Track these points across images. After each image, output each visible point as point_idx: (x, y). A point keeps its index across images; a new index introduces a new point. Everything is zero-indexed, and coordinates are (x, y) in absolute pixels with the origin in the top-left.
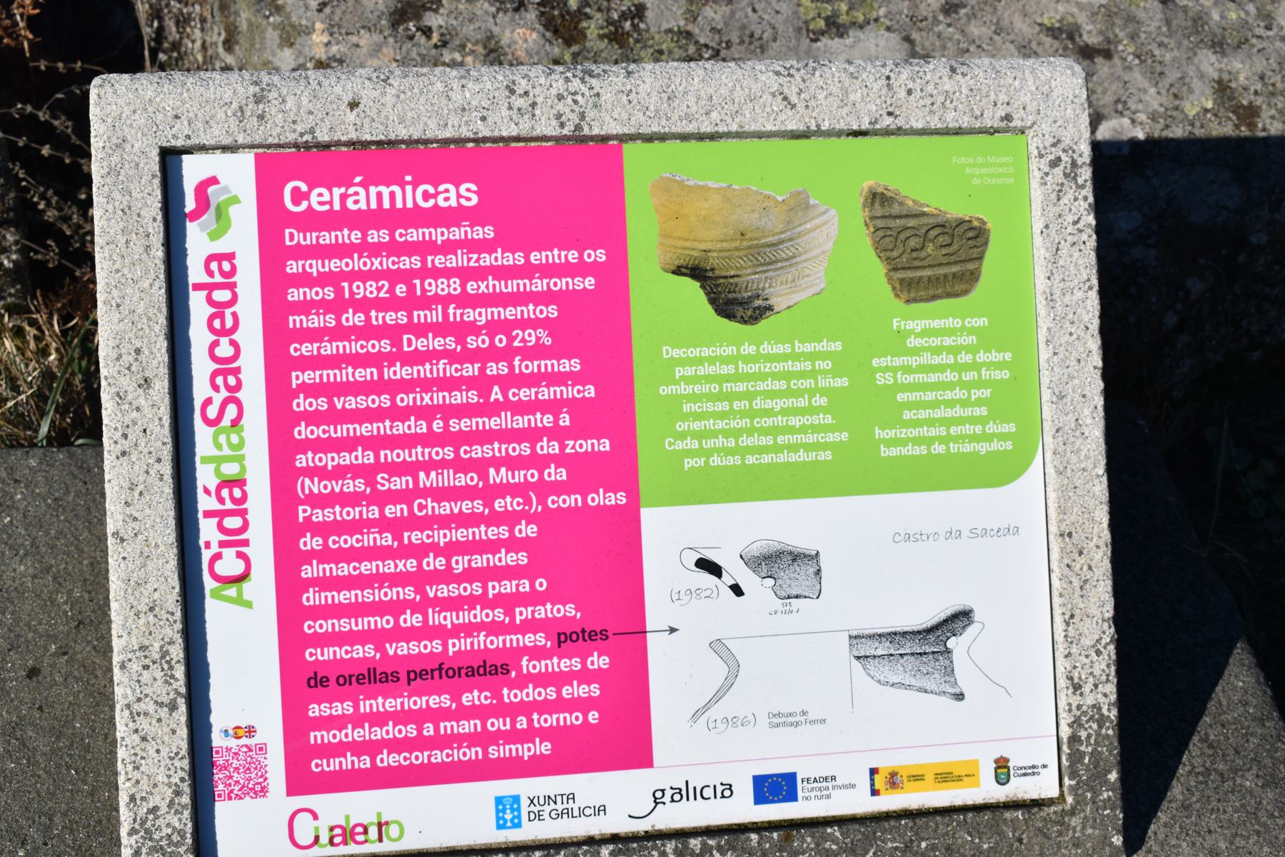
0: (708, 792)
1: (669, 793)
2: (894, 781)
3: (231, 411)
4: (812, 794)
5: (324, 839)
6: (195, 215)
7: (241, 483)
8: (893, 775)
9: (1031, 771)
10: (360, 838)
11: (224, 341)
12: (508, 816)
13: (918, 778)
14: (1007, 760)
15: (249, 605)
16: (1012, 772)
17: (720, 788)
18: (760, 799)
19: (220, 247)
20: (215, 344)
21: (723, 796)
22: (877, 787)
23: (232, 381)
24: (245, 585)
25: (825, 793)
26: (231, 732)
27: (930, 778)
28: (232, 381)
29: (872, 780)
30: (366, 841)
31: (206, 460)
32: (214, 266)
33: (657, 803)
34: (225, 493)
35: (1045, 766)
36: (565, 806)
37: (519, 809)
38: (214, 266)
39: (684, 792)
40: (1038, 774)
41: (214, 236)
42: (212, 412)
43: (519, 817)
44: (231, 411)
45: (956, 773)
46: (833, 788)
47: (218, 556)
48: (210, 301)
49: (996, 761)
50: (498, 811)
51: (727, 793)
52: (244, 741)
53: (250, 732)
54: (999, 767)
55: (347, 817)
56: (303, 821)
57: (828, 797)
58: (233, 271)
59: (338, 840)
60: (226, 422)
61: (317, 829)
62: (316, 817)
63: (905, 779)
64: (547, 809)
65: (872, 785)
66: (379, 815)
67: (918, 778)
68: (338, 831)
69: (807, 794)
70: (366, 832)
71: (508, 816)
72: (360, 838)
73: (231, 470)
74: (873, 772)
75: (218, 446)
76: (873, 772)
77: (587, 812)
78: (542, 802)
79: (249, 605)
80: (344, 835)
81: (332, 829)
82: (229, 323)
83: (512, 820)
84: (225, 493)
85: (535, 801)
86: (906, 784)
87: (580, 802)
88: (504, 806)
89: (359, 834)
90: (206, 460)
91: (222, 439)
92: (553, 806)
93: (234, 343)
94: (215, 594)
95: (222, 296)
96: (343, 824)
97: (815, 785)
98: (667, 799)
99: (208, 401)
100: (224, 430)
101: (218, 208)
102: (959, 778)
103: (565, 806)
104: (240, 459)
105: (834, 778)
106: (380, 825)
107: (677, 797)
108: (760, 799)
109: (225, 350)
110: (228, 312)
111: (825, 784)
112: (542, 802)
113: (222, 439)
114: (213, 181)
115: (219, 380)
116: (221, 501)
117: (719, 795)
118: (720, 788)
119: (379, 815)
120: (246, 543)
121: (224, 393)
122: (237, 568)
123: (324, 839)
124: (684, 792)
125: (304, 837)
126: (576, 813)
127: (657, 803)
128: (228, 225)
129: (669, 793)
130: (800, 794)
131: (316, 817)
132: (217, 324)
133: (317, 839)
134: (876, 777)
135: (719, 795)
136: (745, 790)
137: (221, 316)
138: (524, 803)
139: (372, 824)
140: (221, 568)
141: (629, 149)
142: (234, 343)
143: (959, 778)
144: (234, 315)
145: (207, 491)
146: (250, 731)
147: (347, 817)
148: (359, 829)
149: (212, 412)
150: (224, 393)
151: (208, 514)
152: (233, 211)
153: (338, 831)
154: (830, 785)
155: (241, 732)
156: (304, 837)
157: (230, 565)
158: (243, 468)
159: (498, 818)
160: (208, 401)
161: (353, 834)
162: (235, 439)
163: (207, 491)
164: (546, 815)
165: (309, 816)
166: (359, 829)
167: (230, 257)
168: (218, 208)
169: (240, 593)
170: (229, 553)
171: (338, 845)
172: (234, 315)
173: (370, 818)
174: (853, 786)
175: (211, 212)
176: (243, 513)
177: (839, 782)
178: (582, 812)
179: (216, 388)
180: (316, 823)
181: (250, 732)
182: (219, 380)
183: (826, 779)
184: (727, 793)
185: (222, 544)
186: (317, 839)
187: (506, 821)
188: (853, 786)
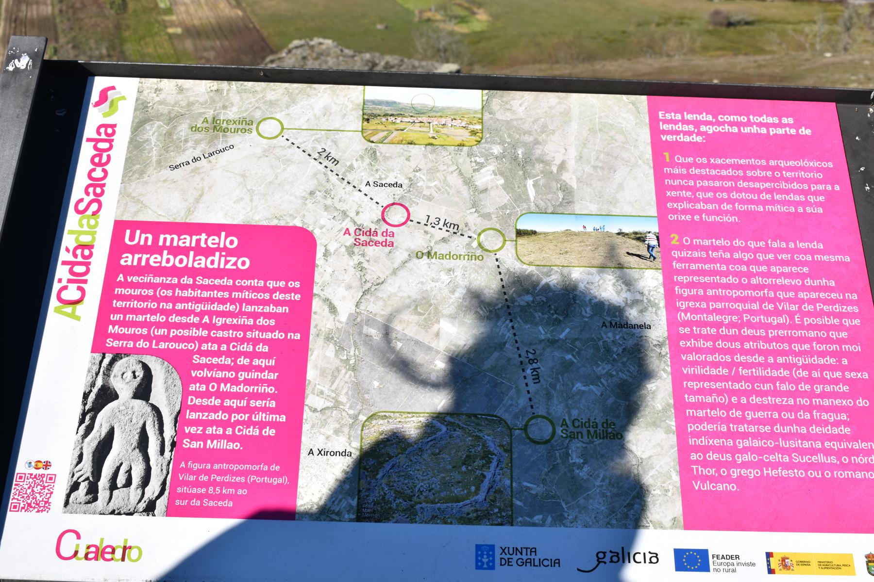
1: (608, 555)
3: (94, 207)
4: (721, 567)
6: (97, 104)
7: (90, 247)
10: (107, 556)
11: (99, 169)
12: (485, 560)
13: (804, 563)
15: (78, 318)
17: (648, 556)
20: (93, 170)
21: (651, 562)
22: (772, 567)
23: (98, 190)
24: (79, 307)
25: (731, 567)
26: (33, 464)
27: (814, 564)
28: (98, 190)
29: (768, 561)
30: (112, 559)
31: (71, 232)
32: (102, 130)
33: (599, 562)
34: (79, 252)
37: (493, 556)
38: (102, 130)
39: (620, 556)
41: (105, 115)
42: (82, 207)
44: (94, 207)
45: (835, 562)
46: (738, 564)
48: (95, 148)
49: (867, 556)
50: (477, 556)
52: (41, 471)
53: (46, 466)
54: (870, 561)
55: (102, 540)
57: (734, 571)
59: (91, 556)
61: (78, 545)
62: (79, 537)
63: (795, 564)
64: (515, 557)
65: (769, 565)
66: (126, 540)
67: (804, 563)
68: (93, 549)
69: (717, 567)
70: (113, 552)
71: (485, 560)
72: (107, 556)
73: (85, 239)
75: (81, 225)
76: (769, 555)
77: (546, 563)
78: (511, 552)
79: (78, 318)
80: (96, 553)
82: (104, 159)
84: (79, 252)
85: (506, 551)
87: (540, 555)
90: (71, 232)
91: (85, 221)
92: (519, 556)
94: (57, 310)
95: (103, 145)
96: (98, 544)
98: (607, 559)
99: (81, 200)
100: (88, 217)
101: (112, 102)
102: (838, 567)
103: (529, 556)
104: (93, 234)
105: (737, 557)
106: (125, 549)
107: (615, 559)
109: (98, 173)
110: (105, 155)
111: (730, 561)
112: (511, 552)
114: (113, 88)
115: (91, 190)
116: (75, 256)
118: (648, 556)
119: (126, 540)
120: (85, 282)
121: (92, 197)
122: (77, 295)
123: (82, 554)
124: (620, 556)
125: (66, 551)
126: (537, 563)
127: (599, 562)
128: (116, 110)
129: (608, 555)
130: (711, 567)
131: (79, 537)
132: (97, 160)
133: (76, 553)
137: (100, 156)
138: (498, 551)
139: (119, 547)
140: (65, 295)
141: (366, 98)
143: (838, 567)
144: (109, 156)
145: (67, 250)
146: (47, 465)
147: (102, 540)
149: (82, 207)
150: (92, 197)
151: (64, 263)
152: (121, 104)
154: (735, 561)
155: (40, 465)
156: (66, 551)
157: (72, 293)
158: (94, 239)
160: (81, 200)
161: (103, 552)
162: (92, 222)
163: (67, 250)
164: (514, 562)
165: (74, 535)
166: (109, 550)
167: (113, 126)
168: (112, 102)
169: (74, 311)
170: (73, 287)
171: (91, 559)
172: (109, 156)
173: (118, 543)
174: (754, 565)
175: (107, 103)
176: (87, 265)
177: (742, 560)
179: (87, 194)
181: (46, 466)
182: (91, 190)
183: (731, 557)
185: (69, 281)
186: (76, 553)
188: (754, 565)
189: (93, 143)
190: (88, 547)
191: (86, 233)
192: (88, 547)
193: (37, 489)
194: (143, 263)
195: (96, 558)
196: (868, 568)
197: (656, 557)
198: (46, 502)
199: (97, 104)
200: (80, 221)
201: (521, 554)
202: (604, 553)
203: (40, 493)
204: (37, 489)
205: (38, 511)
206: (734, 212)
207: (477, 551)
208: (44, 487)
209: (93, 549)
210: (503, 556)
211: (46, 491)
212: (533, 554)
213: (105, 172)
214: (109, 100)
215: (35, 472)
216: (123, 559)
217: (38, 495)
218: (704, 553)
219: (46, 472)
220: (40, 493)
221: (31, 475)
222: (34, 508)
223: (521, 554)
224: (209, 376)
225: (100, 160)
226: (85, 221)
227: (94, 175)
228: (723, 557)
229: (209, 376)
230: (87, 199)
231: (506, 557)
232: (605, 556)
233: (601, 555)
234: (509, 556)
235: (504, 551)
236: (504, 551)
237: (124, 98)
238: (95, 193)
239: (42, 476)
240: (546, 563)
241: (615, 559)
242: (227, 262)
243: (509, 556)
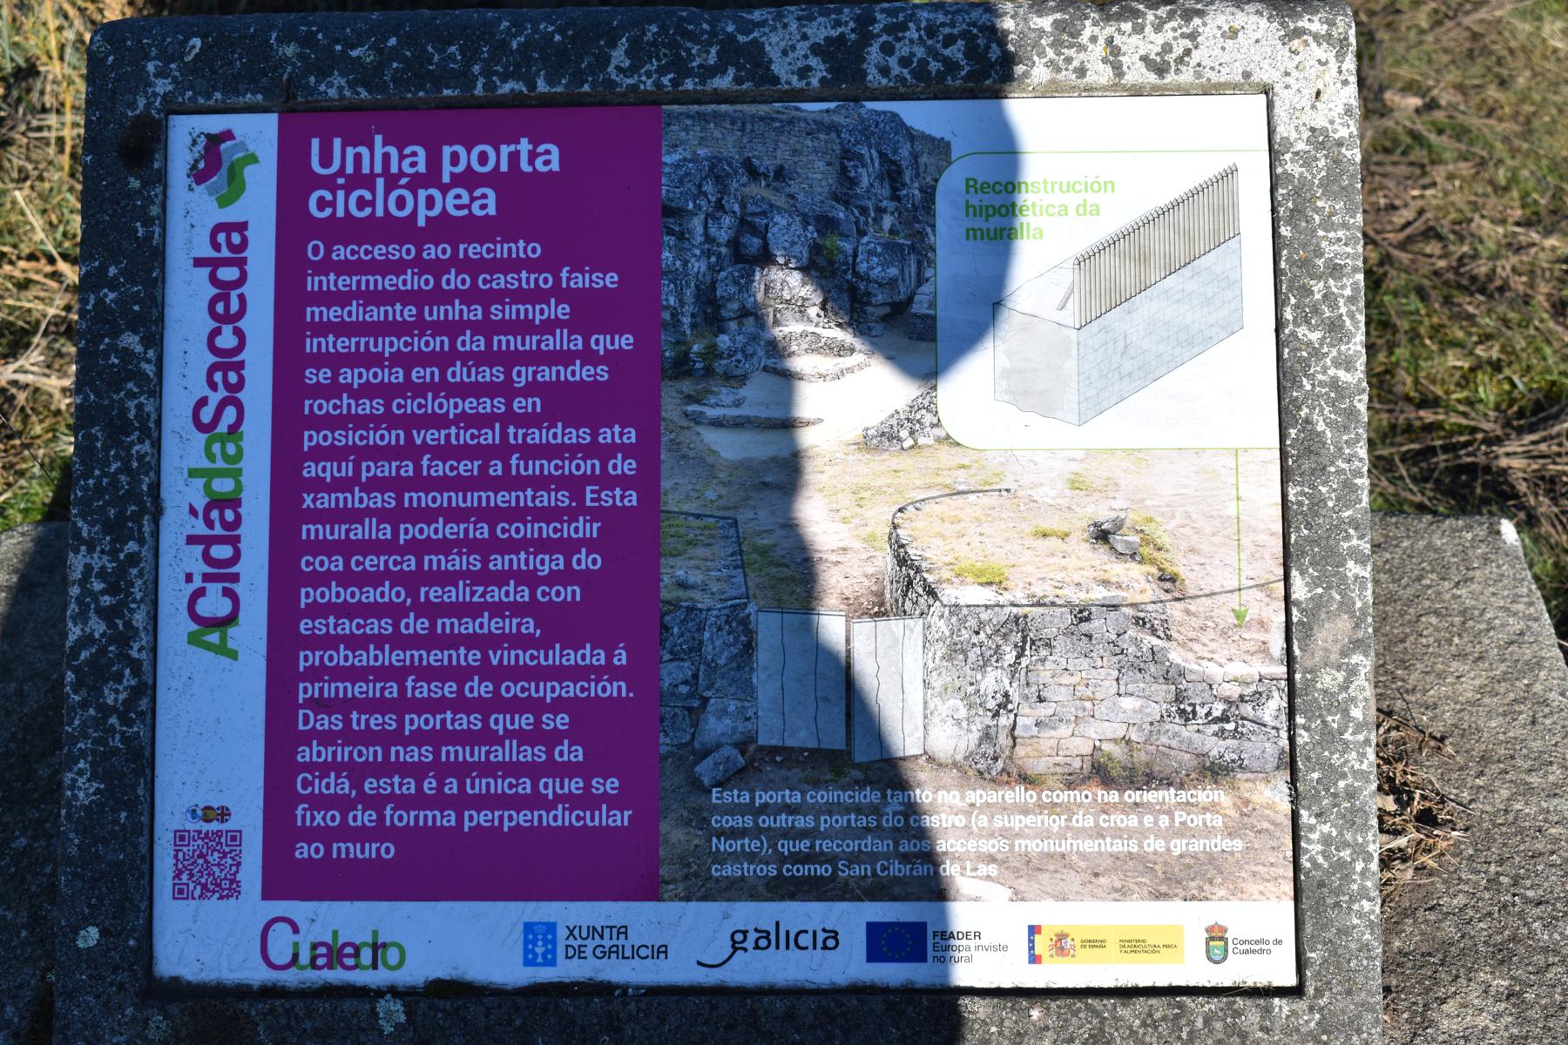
0: (805, 940)
1: (752, 936)
2: (1061, 945)
5: (305, 958)
7: (235, 503)
8: (1061, 937)
9: (1257, 947)
10: (350, 962)
11: (227, 330)
12: (540, 950)
13: (1097, 944)
15: (233, 655)
16: (1231, 946)
17: (821, 936)
19: (231, 215)
20: (216, 332)
21: (825, 947)
22: (1037, 952)
23: (233, 378)
24: (232, 631)
26: (199, 812)
28: (233, 378)
29: (1031, 941)
32: (221, 238)
33: (735, 949)
34: (215, 514)
35: (1279, 942)
36: (614, 942)
37: (554, 942)
38: (221, 238)
39: (773, 937)
40: (1269, 952)
41: (224, 202)
43: (554, 952)
44: (230, 414)
46: (977, 948)
47: (200, 593)
48: (213, 279)
50: (526, 941)
51: (831, 943)
52: (215, 826)
53: (222, 815)
54: (1212, 939)
55: (335, 933)
56: (281, 933)
58: (244, 244)
60: (222, 428)
61: (296, 945)
62: (296, 930)
63: (1078, 944)
64: (591, 944)
65: (1031, 948)
66: (375, 933)
67: (1097, 944)
68: (323, 950)
70: (357, 954)
71: (540, 950)
72: (350, 962)
73: (224, 486)
75: (211, 457)
76: (1034, 930)
77: (643, 952)
78: (584, 934)
79: (233, 655)
80: (329, 955)
81: (315, 946)
82: (235, 306)
83: (544, 956)
84: (215, 514)
85: (576, 932)
86: (1080, 952)
87: (634, 939)
88: (535, 935)
89: (349, 956)
91: (216, 448)
92: (598, 941)
93: (239, 333)
95: (228, 274)
96: (329, 940)
98: (749, 944)
99: (203, 402)
100: (223, 440)
102: (1155, 949)
103: (614, 942)
104: (236, 474)
105: (978, 935)
106: (375, 947)
107: (763, 943)
109: (227, 340)
110: (234, 294)
113: (216, 448)
114: (228, 135)
115: (218, 377)
116: (209, 524)
117: (820, 944)
118: (821, 936)
119: (375, 933)
122: (225, 607)
123: (305, 958)
124: (773, 937)
126: (628, 953)
127: (735, 949)
128: (242, 190)
129: (752, 936)
130: (930, 958)
131: (296, 930)
132: (220, 308)
133: (295, 957)
135: (820, 944)
136: (855, 942)
137: (225, 298)
138: (562, 933)
139: (365, 944)
143: (1155, 949)
144: (242, 298)
145: (193, 512)
147: (335, 933)
148: (349, 950)
150: (222, 393)
152: (249, 171)
153: (323, 950)
154: (972, 943)
155: (211, 815)
158: (239, 487)
159: (526, 951)
160: (203, 402)
161: (341, 955)
162: (231, 449)
164: (588, 951)
165: (287, 928)
167: (242, 227)
169: (223, 639)
170: (214, 589)
172: (242, 298)
174: (1004, 948)
177: (985, 941)
178: (635, 951)
179: (213, 386)
180: (296, 938)
181: (222, 815)
182: (218, 377)
184: (831, 943)
185: (207, 578)
186: (295, 957)
187: (536, 955)
188: (1004, 948)
191: (222, 473)
193: (214, 857)
194: (362, 349)
196: (1208, 951)
201: (602, 937)
203: (218, 865)
204: (214, 857)
205: (221, 898)
206: (379, 832)
208: (225, 855)
210: (571, 941)
211: (230, 861)
212: (622, 937)
213: (239, 333)
214: (225, 166)
215: (205, 827)
216: (375, 966)
217: (215, 869)
219: (224, 827)
220: (218, 865)
221: (199, 832)
222: (214, 892)
223: (602, 937)
225: (227, 307)
230: (215, 398)
231: (576, 944)
232: (825, 941)
233: (739, 937)
234: (580, 942)
235: (571, 933)
236: (571, 933)
237: (253, 159)
239: (218, 834)
240: (643, 952)
241: (763, 943)
243: (580, 942)
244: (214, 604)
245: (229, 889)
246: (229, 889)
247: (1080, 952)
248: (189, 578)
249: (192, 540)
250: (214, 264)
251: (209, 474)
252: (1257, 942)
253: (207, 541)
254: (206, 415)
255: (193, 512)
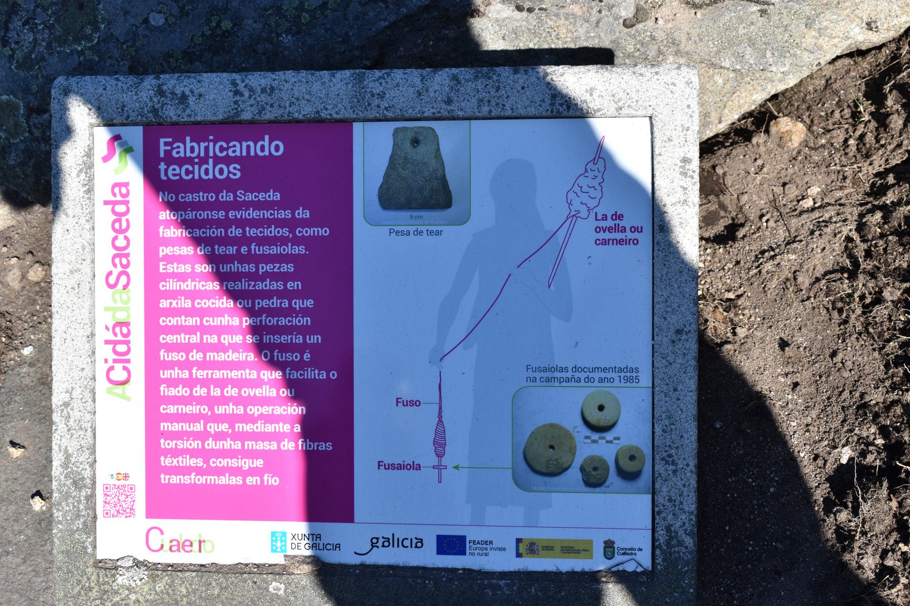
1: (381, 540)
4: (476, 552)
5: (166, 547)
7: (127, 324)
10: (188, 549)
11: (121, 236)
12: (279, 544)
14: (613, 543)
15: (128, 399)
17: (414, 541)
18: (441, 551)
20: (116, 238)
21: (416, 547)
23: (124, 261)
24: (126, 386)
26: (115, 476)
27: (558, 549)
28: (124, 261)
29: (517, 547)
33: (373, 547)
35: (640, 550)
37: (285, 541)
38: (117, 190)
39: (391, 541)
43: (285, 546)
44: (123, 280)
46: (491, 549)
47: (112, 368)
49: (605, 542)
50: (272, 541)
51: (419, 545)
52: (122, 482)
55: (181, 535)
57: (486, 555)
59: (174, 548)
62: (162, 533)
63: (540, 548)
65: (517, 549)
68: (175, 543)
70: (191, 545)
71: (279, 544)
73: (121, 317)
74: (519, 541)
76: (519, 541)
79: (128, 399)
80: (178, 545)
82: (124, 226)
84: (118, 330)
86: (541, 552)
93: (126, 238)
95: (120, 208)
97: (478, 546)
98: (380, 544)
99: (110, 273)
102: (578, 552)
104: (127, 310)
105: (491, 542)
106: (200, 542)
107: (386, 544)
108: (441, 551)
109: (121, 242)
110: (124, 219)
111: (485, 546)
113: (117, 296)
115: (117, 260)
116: (115, 334)
117: (414, 545)
118: (414, 541)
120: (128, 361)
121: (119, 269)
123: (166, 547)
124: (391, 541)
126: (321, 547)
127: (373, 547)
129: (381, 540)
130: (468, 551)
131: (162, 533)
132: (117, 226)
133: (162, 546)
134: (521, 545)
135: (414, 545)
136: (431, 544)
137: (119, 221)
142: (126, 238)
143: (578, 552)
144: (127, 221)
145: (107, 328)
146: (126, 477)
147: (181, 535)
150: (119, 269)
154: (488, 547)
155: (121, 477)
158: (129, 315)
159: (272, 545)
161: (184, 546)
162: (124, 297)
165: (158, 532)
166: (188, 543)
172: (127, 221)
174: (505, 549)
179: (115, 265)
184: (419, 545)
185: (115, 361)
186: (162, 546)
188: (505, 549)
189: (111, 206)
190: (171, 542)
191: (121, 309)
192: (171, 542)
195: (178, 550)
197: (421, 542)
198: (131, 509)
199: (106, 159)
200: (113, 295)
202: (377, 539)
204: (123, 498)
207: (272, 537)
209: (175, 543)
210: (294, 541)
216: (200, 551)
218: (462, 539)
224: (252, 394)
226: (117, 296)
227: (118, 243)
228: (478, 543)
229: (252, 394)
230: (116, 272)
231: (296, 542)
233: (375, 541)
238: (122, 266)
239: (124, 486)
241: (386, 544)
242: (249, 285)
244: (119, 374)
245: (131, 512)
246: (131, 512)
247: (541, 552)
248: (106, 361)
249: (107, 342)
250: (114, 203)
251: (114, 310)
252: (629, 549)
253: (115, 343)
254: (112, 280)
255: (107, 328)
